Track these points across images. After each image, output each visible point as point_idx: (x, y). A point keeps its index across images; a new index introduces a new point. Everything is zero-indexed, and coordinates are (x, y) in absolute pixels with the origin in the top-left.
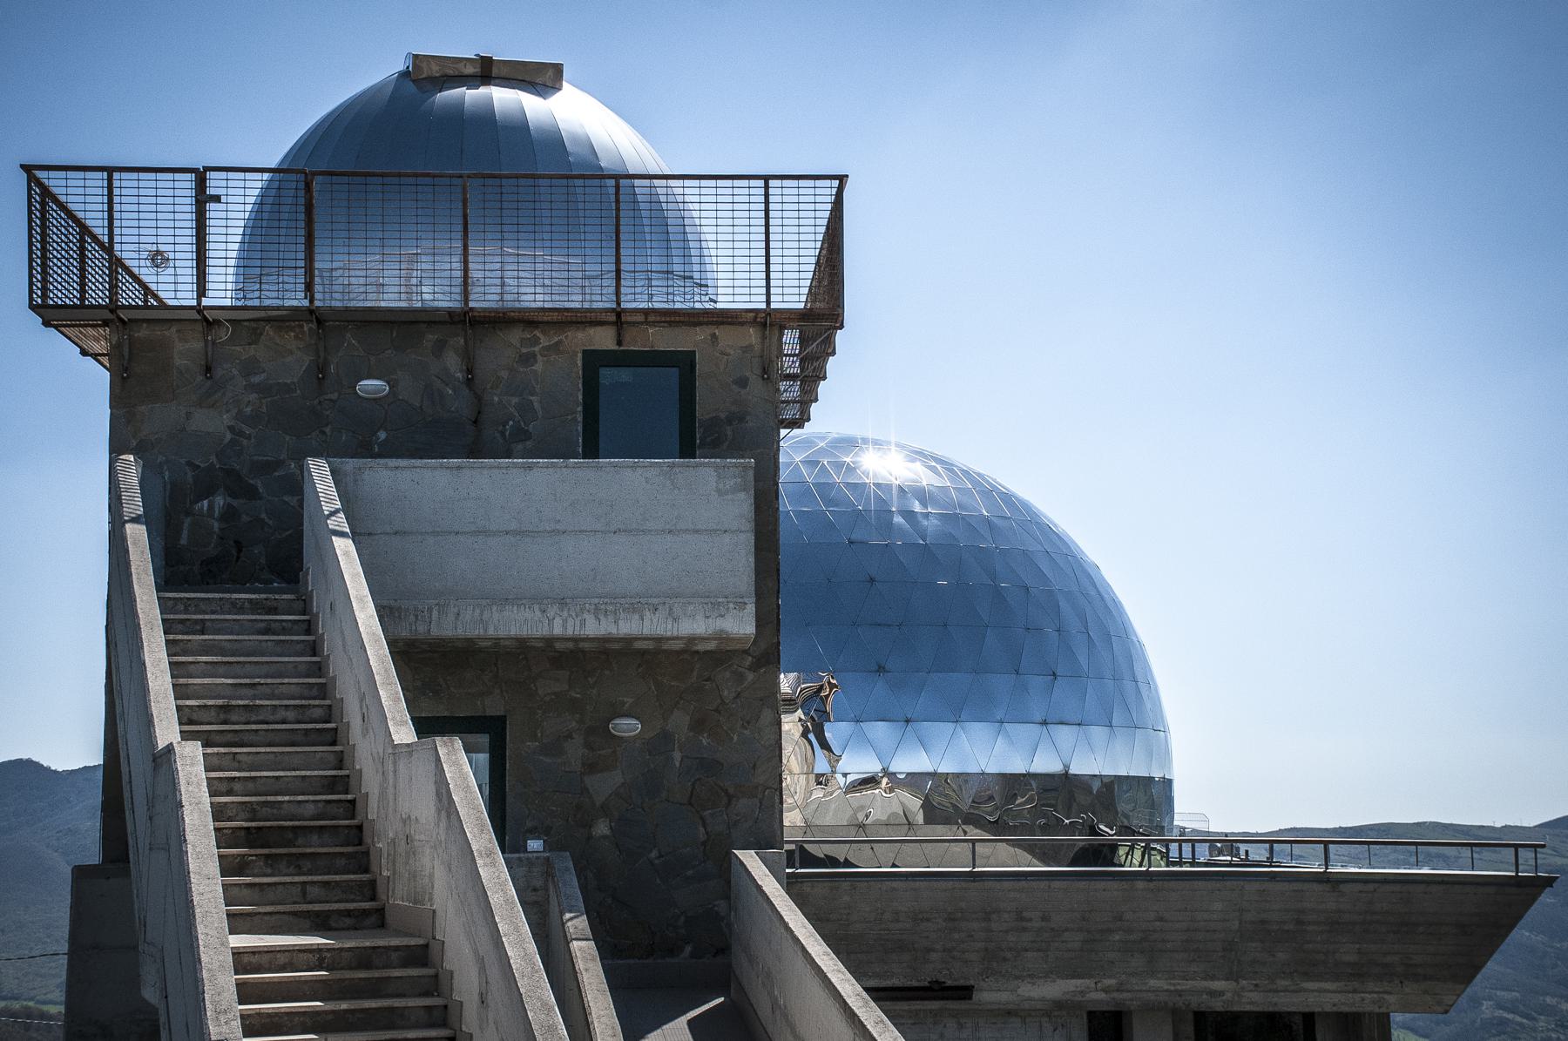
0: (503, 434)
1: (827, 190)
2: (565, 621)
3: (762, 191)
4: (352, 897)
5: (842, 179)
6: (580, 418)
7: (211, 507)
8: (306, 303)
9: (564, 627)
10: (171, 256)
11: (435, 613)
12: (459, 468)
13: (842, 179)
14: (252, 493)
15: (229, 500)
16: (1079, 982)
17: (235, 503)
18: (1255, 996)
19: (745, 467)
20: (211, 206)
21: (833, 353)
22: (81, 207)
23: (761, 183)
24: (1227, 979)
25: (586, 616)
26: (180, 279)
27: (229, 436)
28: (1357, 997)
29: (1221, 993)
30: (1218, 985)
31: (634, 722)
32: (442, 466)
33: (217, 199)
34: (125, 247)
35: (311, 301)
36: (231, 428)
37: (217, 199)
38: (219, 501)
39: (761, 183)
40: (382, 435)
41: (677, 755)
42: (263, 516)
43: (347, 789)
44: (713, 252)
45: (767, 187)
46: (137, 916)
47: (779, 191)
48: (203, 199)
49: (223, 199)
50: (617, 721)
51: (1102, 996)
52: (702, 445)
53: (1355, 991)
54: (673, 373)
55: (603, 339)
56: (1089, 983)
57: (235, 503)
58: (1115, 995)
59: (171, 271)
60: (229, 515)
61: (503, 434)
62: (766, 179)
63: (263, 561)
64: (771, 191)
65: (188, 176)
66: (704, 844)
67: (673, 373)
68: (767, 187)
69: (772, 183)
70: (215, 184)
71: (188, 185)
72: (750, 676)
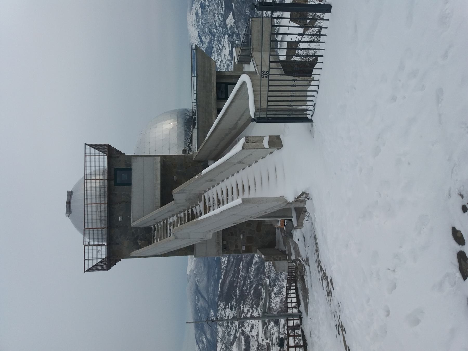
0: (128, 198)
1: (87, 146)
2: (158, 186)
3: (87, 157)
4: (239, 58)
5: (85, 144)
6: (125, 186)
7: (140, 243)
8: (106, 229)
9: (159, 186)
10: (98, 250)
11: (156, 206)
12: (133, 203)
13: (85, 144)
14: (138, 236)
15: (139, 240)
16: (213, 115)
17: (139, 239)
18: (214, 89)
19: (133, 158)
20: (90, 244)
21: (116, 148)
22: (89, 267)
23: (86, 157)
24: (212, 93)
25: (157, 183)
26: (102, 248)
27: (128, 240)
28: (214, 74)
29: (214, 94)
30: (213, 94)
31: (174, 177)
32: (133, 206)
33: (89, 243)
34: (103, 256)
35: (106, 228)
36: (127, 240)
37: (89, 243)
38: (139, 241)
39: (86, 157)
40: (128, 217)
41: (180, 170)
42: (141, 234)
43: (298, 326)
44: (103, 167)
45: (87, 156)
46: (200, 241)
47: (87, 154)
48: (89, 245)
49: (89, 242)
50: (174, 179)
51: (215, 111)
52: (130, 167)
53: (213, 74)
54: (118, 171)
55: (113, 182)
56: (213, 113)
57: (139, 239)
58: (215, 109)
59: (101, 250)
60: (141, 240)
61: (128, 198)
62: (85, 156)
63: (148, 234)
64: (87, 155)
65: (85, 248)
66: (193, 166)
67: (118, 171)
68: (87, 156)
69: (86, 155)
70: (86, 243)
71: (87, 248)
72: (167, 159)
